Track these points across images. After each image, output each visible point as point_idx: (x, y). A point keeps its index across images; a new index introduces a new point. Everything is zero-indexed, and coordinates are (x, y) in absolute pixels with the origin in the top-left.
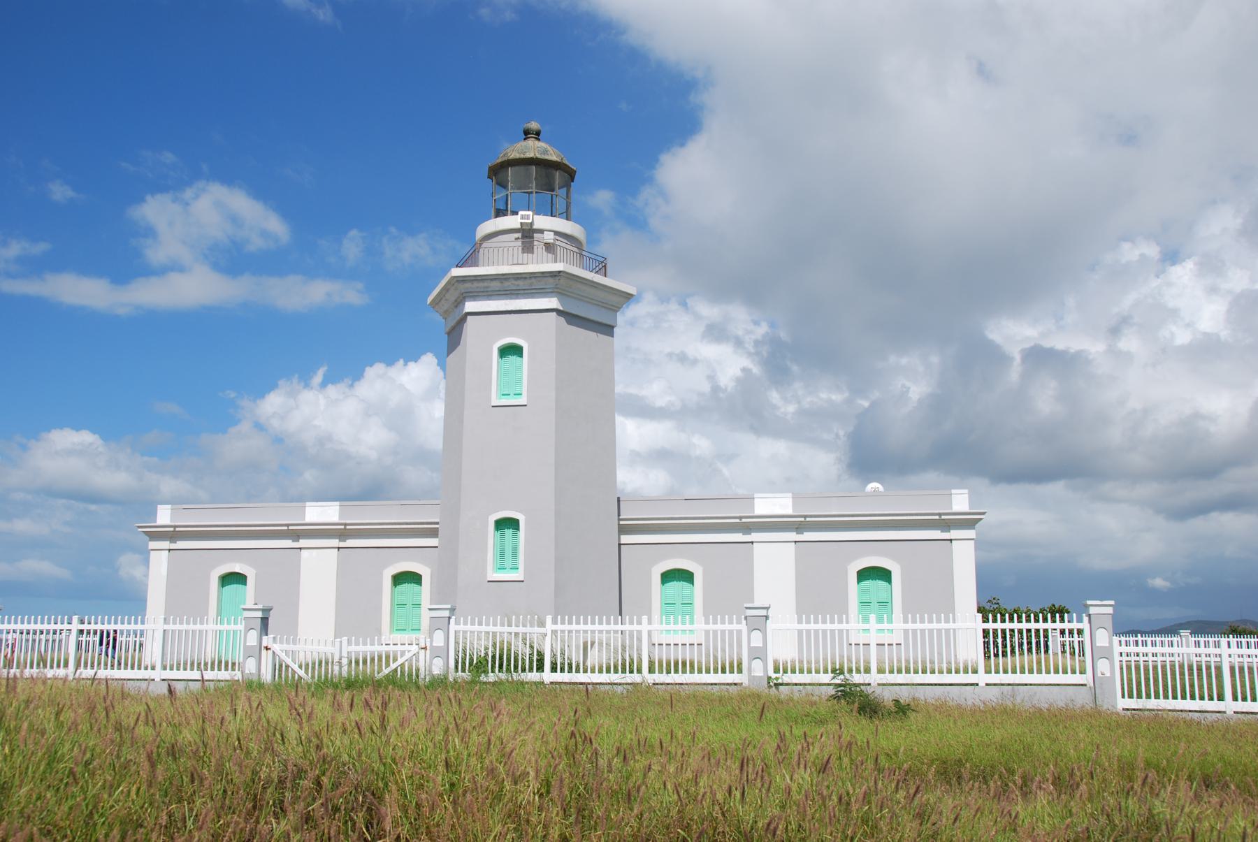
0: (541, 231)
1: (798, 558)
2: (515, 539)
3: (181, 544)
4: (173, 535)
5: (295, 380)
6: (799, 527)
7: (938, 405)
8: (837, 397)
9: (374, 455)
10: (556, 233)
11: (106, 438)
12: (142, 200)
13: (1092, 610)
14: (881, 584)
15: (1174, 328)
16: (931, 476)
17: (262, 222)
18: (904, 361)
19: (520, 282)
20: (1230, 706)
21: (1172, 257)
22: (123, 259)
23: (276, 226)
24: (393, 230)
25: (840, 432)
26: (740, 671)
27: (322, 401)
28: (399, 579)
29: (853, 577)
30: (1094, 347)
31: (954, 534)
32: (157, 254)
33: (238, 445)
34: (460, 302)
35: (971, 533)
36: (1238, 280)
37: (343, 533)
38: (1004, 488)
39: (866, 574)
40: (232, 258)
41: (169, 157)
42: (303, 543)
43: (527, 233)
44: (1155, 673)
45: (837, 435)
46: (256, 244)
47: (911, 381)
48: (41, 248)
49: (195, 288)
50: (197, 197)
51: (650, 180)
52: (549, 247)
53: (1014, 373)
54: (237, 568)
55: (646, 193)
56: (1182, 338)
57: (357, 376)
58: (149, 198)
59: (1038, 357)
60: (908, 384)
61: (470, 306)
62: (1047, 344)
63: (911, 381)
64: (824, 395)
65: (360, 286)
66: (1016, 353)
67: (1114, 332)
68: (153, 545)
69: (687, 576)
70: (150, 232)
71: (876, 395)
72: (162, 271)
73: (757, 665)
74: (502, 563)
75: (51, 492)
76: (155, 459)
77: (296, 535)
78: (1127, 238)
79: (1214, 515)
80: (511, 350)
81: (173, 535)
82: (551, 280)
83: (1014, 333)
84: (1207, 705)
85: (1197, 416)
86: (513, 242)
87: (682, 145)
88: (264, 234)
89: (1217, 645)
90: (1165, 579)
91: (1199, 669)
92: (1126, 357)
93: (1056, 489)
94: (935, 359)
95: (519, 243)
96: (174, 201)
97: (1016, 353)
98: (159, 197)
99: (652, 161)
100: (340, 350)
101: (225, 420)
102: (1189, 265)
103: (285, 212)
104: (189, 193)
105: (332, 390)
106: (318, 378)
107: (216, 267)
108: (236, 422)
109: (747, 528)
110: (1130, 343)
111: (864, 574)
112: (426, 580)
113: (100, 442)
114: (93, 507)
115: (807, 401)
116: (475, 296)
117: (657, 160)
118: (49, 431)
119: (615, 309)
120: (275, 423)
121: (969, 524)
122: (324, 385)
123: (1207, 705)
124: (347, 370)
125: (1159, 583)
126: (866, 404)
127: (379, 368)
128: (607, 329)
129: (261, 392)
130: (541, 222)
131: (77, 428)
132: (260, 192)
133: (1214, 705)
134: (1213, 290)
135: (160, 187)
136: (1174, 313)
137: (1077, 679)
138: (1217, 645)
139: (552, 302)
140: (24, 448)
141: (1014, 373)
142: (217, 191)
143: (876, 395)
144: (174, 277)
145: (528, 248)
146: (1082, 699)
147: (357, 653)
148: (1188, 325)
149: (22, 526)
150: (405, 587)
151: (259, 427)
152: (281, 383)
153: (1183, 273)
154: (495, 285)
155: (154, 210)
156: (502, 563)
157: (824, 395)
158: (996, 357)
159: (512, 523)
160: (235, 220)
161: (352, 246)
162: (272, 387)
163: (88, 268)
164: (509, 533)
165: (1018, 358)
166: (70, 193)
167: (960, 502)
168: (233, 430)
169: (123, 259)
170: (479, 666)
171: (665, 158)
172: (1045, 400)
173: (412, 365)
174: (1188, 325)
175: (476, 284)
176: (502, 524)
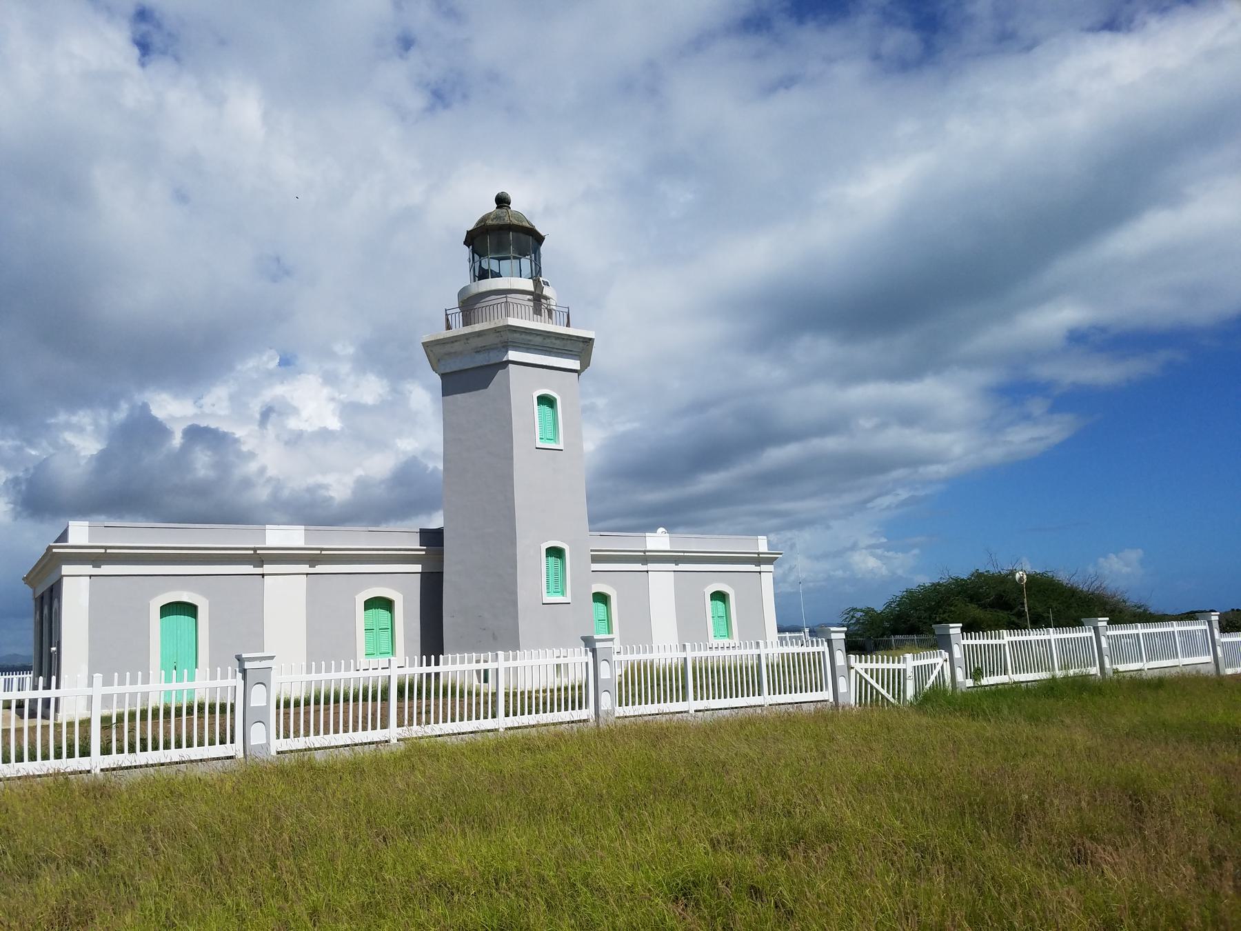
3: (106, 569)
4: (96, 559)
7: (103, 459)
14: (185, 620)
19: (558, 342)
29: (360, 606)
34: (506, 347)
35: (770, 568)
39: (169, 609)
44: (639, 670)
54: (185, 597)
59: (196, 434)
61: (513, 355)
62: (203, 424)
82: (581, 345)
83: (172, 409)
94: (103, 422)
111: (169, 609)
116: (518, 347)
121: (770, 561)
141: (177, 440)
147: (347, 681)
150: (173, 619)
154: (558, 343)
172: (202, 463)
175: (523, 336)
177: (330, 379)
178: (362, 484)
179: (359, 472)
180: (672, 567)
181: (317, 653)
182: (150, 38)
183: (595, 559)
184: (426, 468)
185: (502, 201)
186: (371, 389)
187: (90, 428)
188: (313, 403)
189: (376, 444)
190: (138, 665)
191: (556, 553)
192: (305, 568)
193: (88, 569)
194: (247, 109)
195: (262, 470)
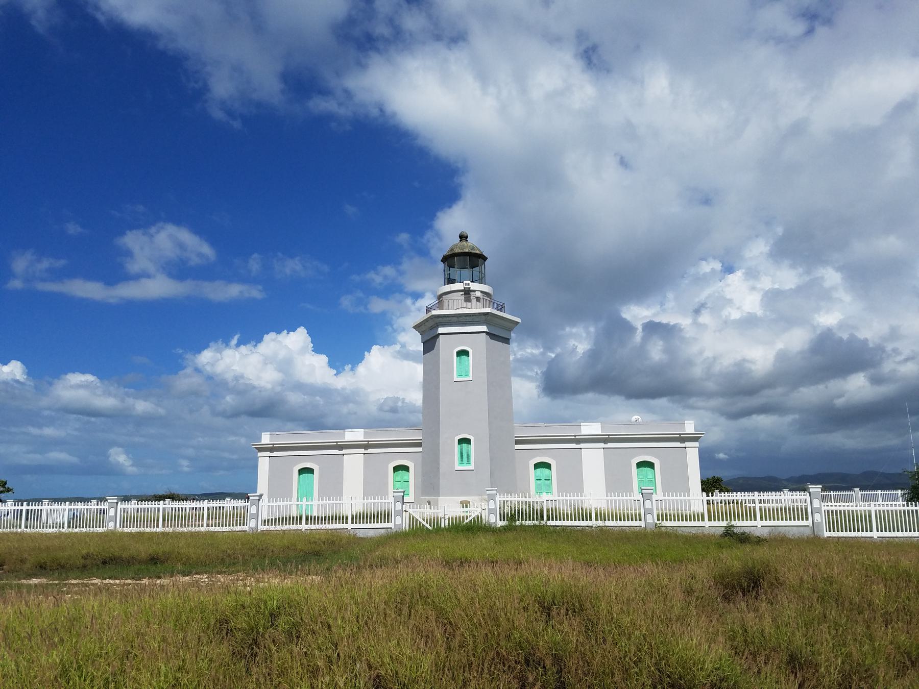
0: (474, 291)
1: (605, 457)
2: (468, 448)
3: (276, 454)
4: (272, 449)
5: (220, 342)
6: (605, 441)
7: (594, 355)
8: (536, 352)
9: (269, 386)
10: (482, 292)
11: (100, 378)
12: (124, 234)
13: (811, 490)
14: (547, 470)
15: (729, 309)
16: (590, 395)
17: (198, 248)
18: (574, 330)
20: (875, 534)
21: (729, 269)
22: (113, 270)
23: (207, 250)
24: (280, 254)
25: (538, 370)
26: (640, 520)
27: (237, 355)
28: (397, 469)
30: (685, 322)
31: (687, 444)
32: (134, 267)
33: (185, 381)
35: (697, 444)
36: (766, 283)
37: (367, 446)
38: (633, 402)
39: (640, 465)
40: (179, 269)
41: (141, 208)
42: (344, 451)
43: (467, 292)
45: (537, 373)
46: (195, 261)
47: (579, 342)
48: (62, 263)
49: (158, 287)
50: (158, 232)
51: (430, 227)
52: (478, 299)
53: (639, 336)
54: (308, 465)
55: (429, 234)
56: (735, 315)
57: (259, 340)
58: (128, 232)
59: (652, 328)
60: (576, 344)
61: (441, 330)
62: (657, 320)
63: (579, 342)
64: (529, 351)
65: (260, 287)
66: (639, 326)
67: (697, 312)
68: (260, 454)
69: (547, 466)
70: (129, 254)
71: (559, 350)
72: (137, 277)
73: (649, 517)
74: (462, 461)
75: (69, 410)
76: (132, 390)
77: (341, 447)
78: (704, 259)
79: (754, 417)
80: (463, 353)
81: (272, 449)
83: (637, 314)
84: (865, 534)
85: (744, 360)
86: (460, 297)
87: (450, 207)
88: (200, 255)
89: (869, 505)
90: (725, 454)
91: (781, 510)
92: (703, 327)
93: (663, 402)
94: (592, 329)
95: (463, 297)
96: (144, 234)
97: (639, 326)
98: (134, 231)
99: (432, 216)
100: (250, 325)
101: (176, 366)
102: (739, 274)
103: (213, 243)
104: (153, 230)
105: (243, 349)
106: (234, 341)
107: (170, 275)
108: (184, 368)
109: (578, 441)
110: (705, 318)
111: (640, 465)
112: (411, 469)
113: (98, 380)
114: (93, 419)
115: (519, 354)
116: (444, 325)
117: (435, 215)
118: (66, 374)
119: (510, 330)
120: (208, 368)
121: (695, 439)
122: (238, 345)
123: (865, 534)
124: (252, 336)
125: (721, 456)
126: (553, 356)
127: (272, 335)
128: (506, 341)
129: (199, 349)
130: (473, 286)
131: (83, 372)
132: (197, 229)
133: (868, 534)
134: (753, 288)
135: (132, 227)
136: (730, 301)
137: (804, 523)
138: (869, 505)
139: (484, 328)
140: (51, 384)
141: (639, 336)
142: (171, 229)
143: (559, 350)
144: (144, 281)
145: (467, 300)
146: (808, 532)
148: (738, 308)
149: (49, 431)
151: (198, 370)
152: (211, 344)
153: (736, 279)
154: (455, 319)
155: (132, 240)
156: (462, 461)
157: (529, 351)
158: (628, 328)
159: (466, 441)
160: (181, 246)
161: (255, 264)
162: (206, 346)
163: (89, 276)
164: (465, 445)
165: (640, 328)
166: (79, 229)
167: (690, 428)
168: (181, 372)
169: (113, 270)
170: (512, 518)
171: (440, 214)
172: (656, 352)
173: (291, 333)
174: (738, 308)
176: (463, 441)
177: (752, 274)
178: (781, 356)
179: (780, 345)
180: (602, 445)
181: (368, 492)
182: (592, 56)
183: (518, 442)
184: (841, 339)
185: (463, 237)
186: (787, 278)
187: (584, 335)
188: (743, 295)
189: (787, 321)
190: (288, 495)
191: (465, 441)
192: (363, 451)
193: (268, 454)
194: (658, 82)
195: (701, 353)
